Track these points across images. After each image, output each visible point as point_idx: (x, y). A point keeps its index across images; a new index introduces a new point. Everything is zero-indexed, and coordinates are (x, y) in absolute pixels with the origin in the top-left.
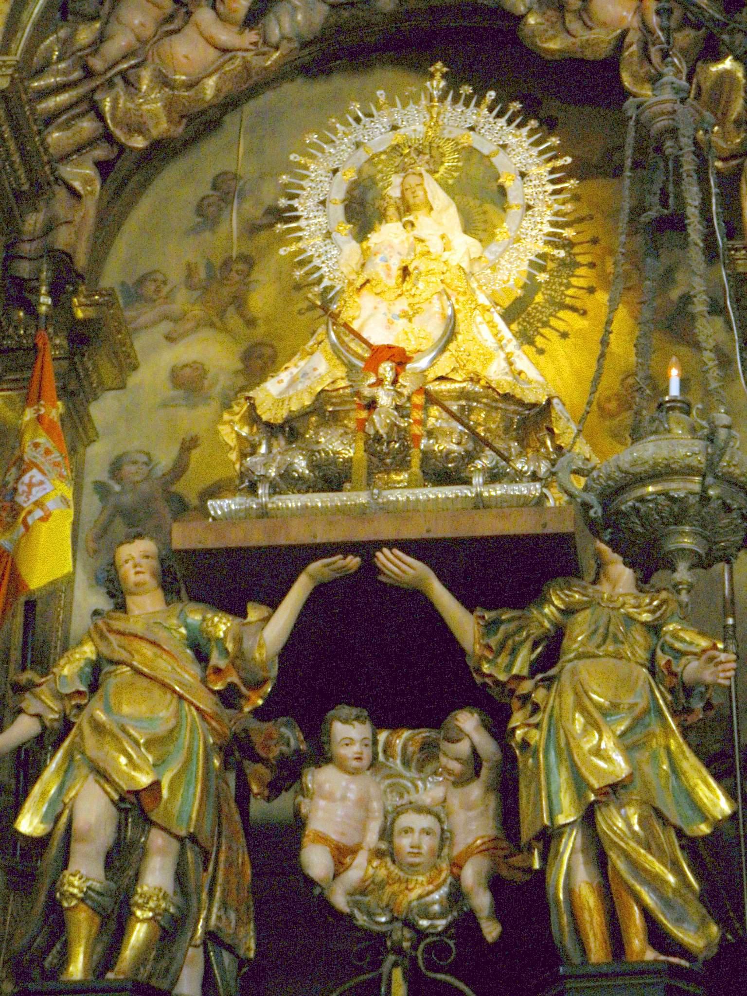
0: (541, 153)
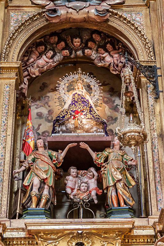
0: (60, 85)
